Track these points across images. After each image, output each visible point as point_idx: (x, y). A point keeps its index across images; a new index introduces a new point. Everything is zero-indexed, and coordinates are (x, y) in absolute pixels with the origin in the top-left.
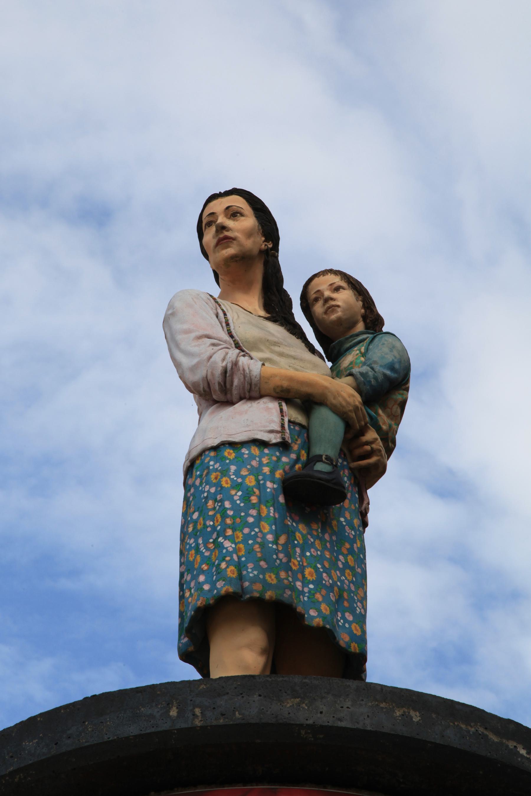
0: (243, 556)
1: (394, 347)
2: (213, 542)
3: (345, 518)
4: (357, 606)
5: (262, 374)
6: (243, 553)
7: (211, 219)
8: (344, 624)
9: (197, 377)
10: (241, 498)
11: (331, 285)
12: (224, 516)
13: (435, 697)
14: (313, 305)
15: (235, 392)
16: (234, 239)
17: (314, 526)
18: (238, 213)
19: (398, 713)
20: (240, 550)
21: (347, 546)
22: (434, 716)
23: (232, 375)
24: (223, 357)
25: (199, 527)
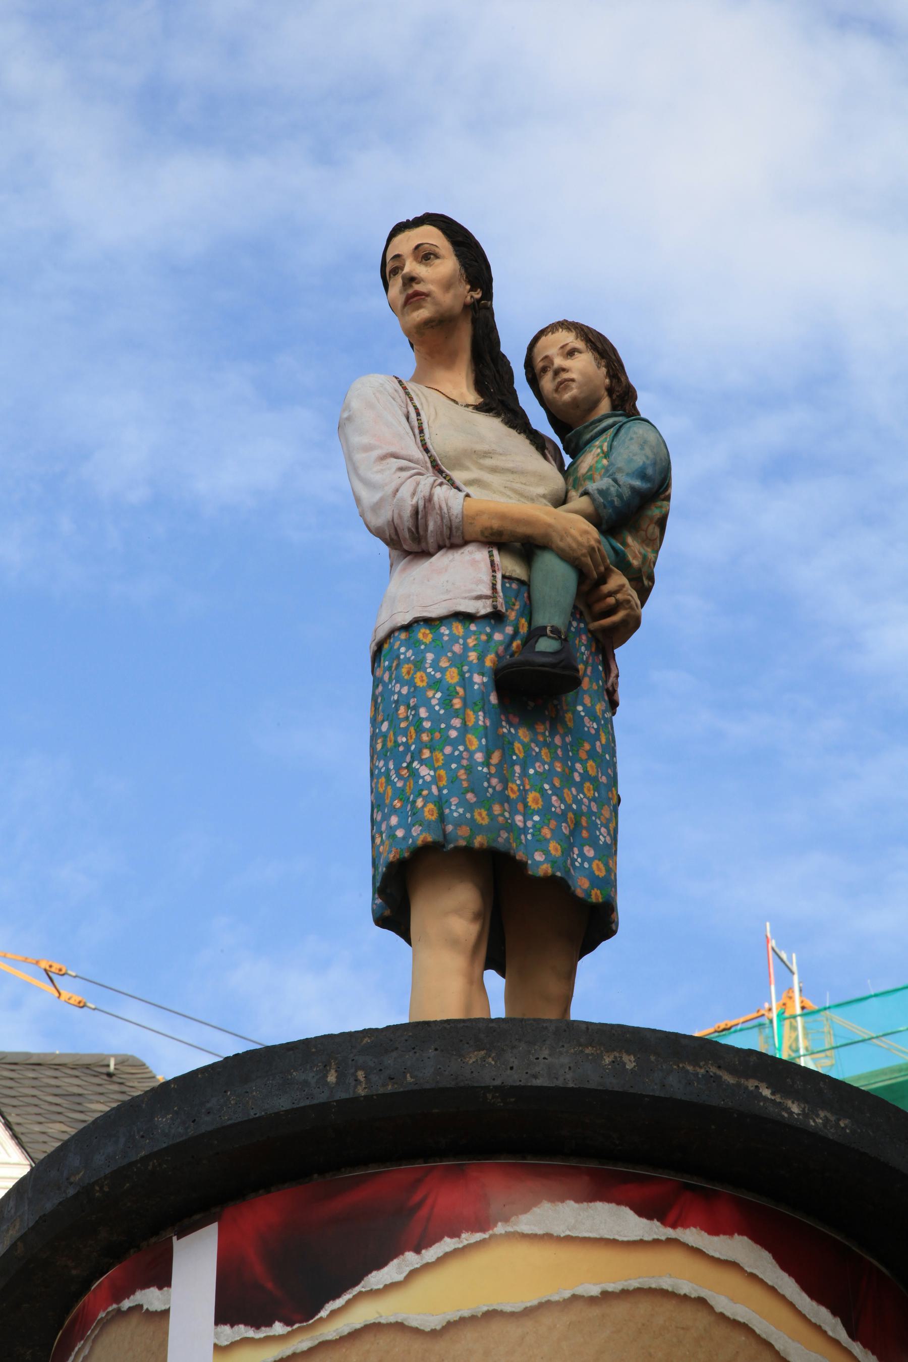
0: (444, 787)
1: (645, 442)
2: (407, 767)
3: (584, 705)
4: (601, 834)
5: (465, 512)
6: (443, 783)
7: (397, 264)
8: (582, 864)
9: (381, 520)
10: (442, 702)
11: (562, 347)
12: (420, 730)
13: (654, 1031)
14: (541, 377)
15: (431, 540)
16: (427, 295)
17: (540, 728)
18: (431, 254)
19: (607, 1060)
20: (440, 778)
21: (587, 746)
22: (653, 1058)
23: (425, 517)
24: (413, 489)
25: (390, 745)
